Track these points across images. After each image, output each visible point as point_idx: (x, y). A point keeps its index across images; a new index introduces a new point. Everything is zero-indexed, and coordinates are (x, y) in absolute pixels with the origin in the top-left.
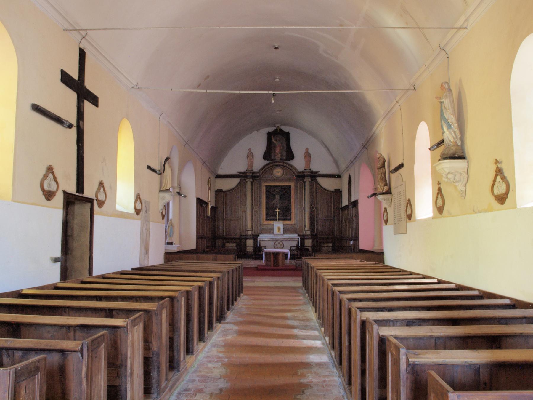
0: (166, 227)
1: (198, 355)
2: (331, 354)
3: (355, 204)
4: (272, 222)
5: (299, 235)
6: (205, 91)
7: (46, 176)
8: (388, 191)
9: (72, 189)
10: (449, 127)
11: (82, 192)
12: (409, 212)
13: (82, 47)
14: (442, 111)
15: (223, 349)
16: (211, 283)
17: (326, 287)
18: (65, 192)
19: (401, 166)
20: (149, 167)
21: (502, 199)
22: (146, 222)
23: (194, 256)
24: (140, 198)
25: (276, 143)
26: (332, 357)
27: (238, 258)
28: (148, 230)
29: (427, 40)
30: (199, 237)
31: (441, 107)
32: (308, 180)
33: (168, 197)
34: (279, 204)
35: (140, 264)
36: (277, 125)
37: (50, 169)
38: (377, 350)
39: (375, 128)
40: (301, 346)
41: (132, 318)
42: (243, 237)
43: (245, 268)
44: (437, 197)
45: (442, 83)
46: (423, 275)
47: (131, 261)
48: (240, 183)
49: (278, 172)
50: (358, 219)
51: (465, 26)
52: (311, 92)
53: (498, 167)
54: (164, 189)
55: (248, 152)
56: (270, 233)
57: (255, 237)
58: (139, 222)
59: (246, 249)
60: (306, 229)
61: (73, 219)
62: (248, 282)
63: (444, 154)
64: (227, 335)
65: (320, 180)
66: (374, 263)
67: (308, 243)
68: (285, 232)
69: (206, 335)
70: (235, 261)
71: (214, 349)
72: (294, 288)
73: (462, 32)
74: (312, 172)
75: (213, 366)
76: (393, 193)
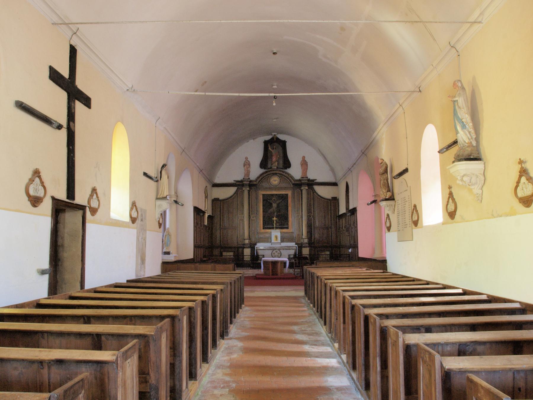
0: (163, 236)
1: (201, 379)
2: (351, 375)
3: (354, 211)
4: (269, 231)
5: (296, 244)
6: (203, 94)
7: (31, 181)
8: (391, 197)
9: (62, 195)
10: (464, 127)
11: (73, 199)
12: (415, 218)
13: (73, 43)
14: (455, 110)
15: (228, 371)
16: (214, 297)
17: (341, 299)
18: (53, 198)
19: (406, 171)
20: (145, 174)
21: (528, 201)
22: (142, 231)
23: (192, 266)
24: (135, 206)
25: (273, 152)
26: (353, 378)
27: (237, 267)
28: (145, 239)
29: (434, 39)
30: (196, 247)
31: (454, 106)
32: (305, 188)
33: (164, 205)
34: (276, 214)
35: (137, 275)
36: (273, 134)
37: (37, 173)
38: (441, 387)
39: (376, 133)
40: (315, 365)
41: (123, 350)
42: (239, 246)
43: (246, 278)
44: (448, 202)
45: (455, 82)
46: (443, 285)
47: (125, 272)
48: (236, 193)
49: (275, 181)
50: (357, 227)
51: (479, 20)
52: (313, 94)
53: (522, 168)
54: (161, 196)
55: (245, 159)
56: (268, 242)
57: (252, 247)
58: (135, 231)
59: (243, 258)
60: (303, 237)
61: (64, 228)
62: (249, 292)
63: (458, 156)
64: (231, 353)
65: (317, 188)
66: (382, 271)
67: (306, 251)
68: (283, 240)
69: (210, 355)
70: (234, 270)
71: (219, 371)
72: (296, 298)
73: (476, 27)
74: (309, 180)
75: (220, 393)
76: (396, 199)
